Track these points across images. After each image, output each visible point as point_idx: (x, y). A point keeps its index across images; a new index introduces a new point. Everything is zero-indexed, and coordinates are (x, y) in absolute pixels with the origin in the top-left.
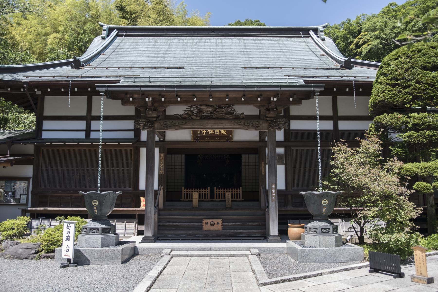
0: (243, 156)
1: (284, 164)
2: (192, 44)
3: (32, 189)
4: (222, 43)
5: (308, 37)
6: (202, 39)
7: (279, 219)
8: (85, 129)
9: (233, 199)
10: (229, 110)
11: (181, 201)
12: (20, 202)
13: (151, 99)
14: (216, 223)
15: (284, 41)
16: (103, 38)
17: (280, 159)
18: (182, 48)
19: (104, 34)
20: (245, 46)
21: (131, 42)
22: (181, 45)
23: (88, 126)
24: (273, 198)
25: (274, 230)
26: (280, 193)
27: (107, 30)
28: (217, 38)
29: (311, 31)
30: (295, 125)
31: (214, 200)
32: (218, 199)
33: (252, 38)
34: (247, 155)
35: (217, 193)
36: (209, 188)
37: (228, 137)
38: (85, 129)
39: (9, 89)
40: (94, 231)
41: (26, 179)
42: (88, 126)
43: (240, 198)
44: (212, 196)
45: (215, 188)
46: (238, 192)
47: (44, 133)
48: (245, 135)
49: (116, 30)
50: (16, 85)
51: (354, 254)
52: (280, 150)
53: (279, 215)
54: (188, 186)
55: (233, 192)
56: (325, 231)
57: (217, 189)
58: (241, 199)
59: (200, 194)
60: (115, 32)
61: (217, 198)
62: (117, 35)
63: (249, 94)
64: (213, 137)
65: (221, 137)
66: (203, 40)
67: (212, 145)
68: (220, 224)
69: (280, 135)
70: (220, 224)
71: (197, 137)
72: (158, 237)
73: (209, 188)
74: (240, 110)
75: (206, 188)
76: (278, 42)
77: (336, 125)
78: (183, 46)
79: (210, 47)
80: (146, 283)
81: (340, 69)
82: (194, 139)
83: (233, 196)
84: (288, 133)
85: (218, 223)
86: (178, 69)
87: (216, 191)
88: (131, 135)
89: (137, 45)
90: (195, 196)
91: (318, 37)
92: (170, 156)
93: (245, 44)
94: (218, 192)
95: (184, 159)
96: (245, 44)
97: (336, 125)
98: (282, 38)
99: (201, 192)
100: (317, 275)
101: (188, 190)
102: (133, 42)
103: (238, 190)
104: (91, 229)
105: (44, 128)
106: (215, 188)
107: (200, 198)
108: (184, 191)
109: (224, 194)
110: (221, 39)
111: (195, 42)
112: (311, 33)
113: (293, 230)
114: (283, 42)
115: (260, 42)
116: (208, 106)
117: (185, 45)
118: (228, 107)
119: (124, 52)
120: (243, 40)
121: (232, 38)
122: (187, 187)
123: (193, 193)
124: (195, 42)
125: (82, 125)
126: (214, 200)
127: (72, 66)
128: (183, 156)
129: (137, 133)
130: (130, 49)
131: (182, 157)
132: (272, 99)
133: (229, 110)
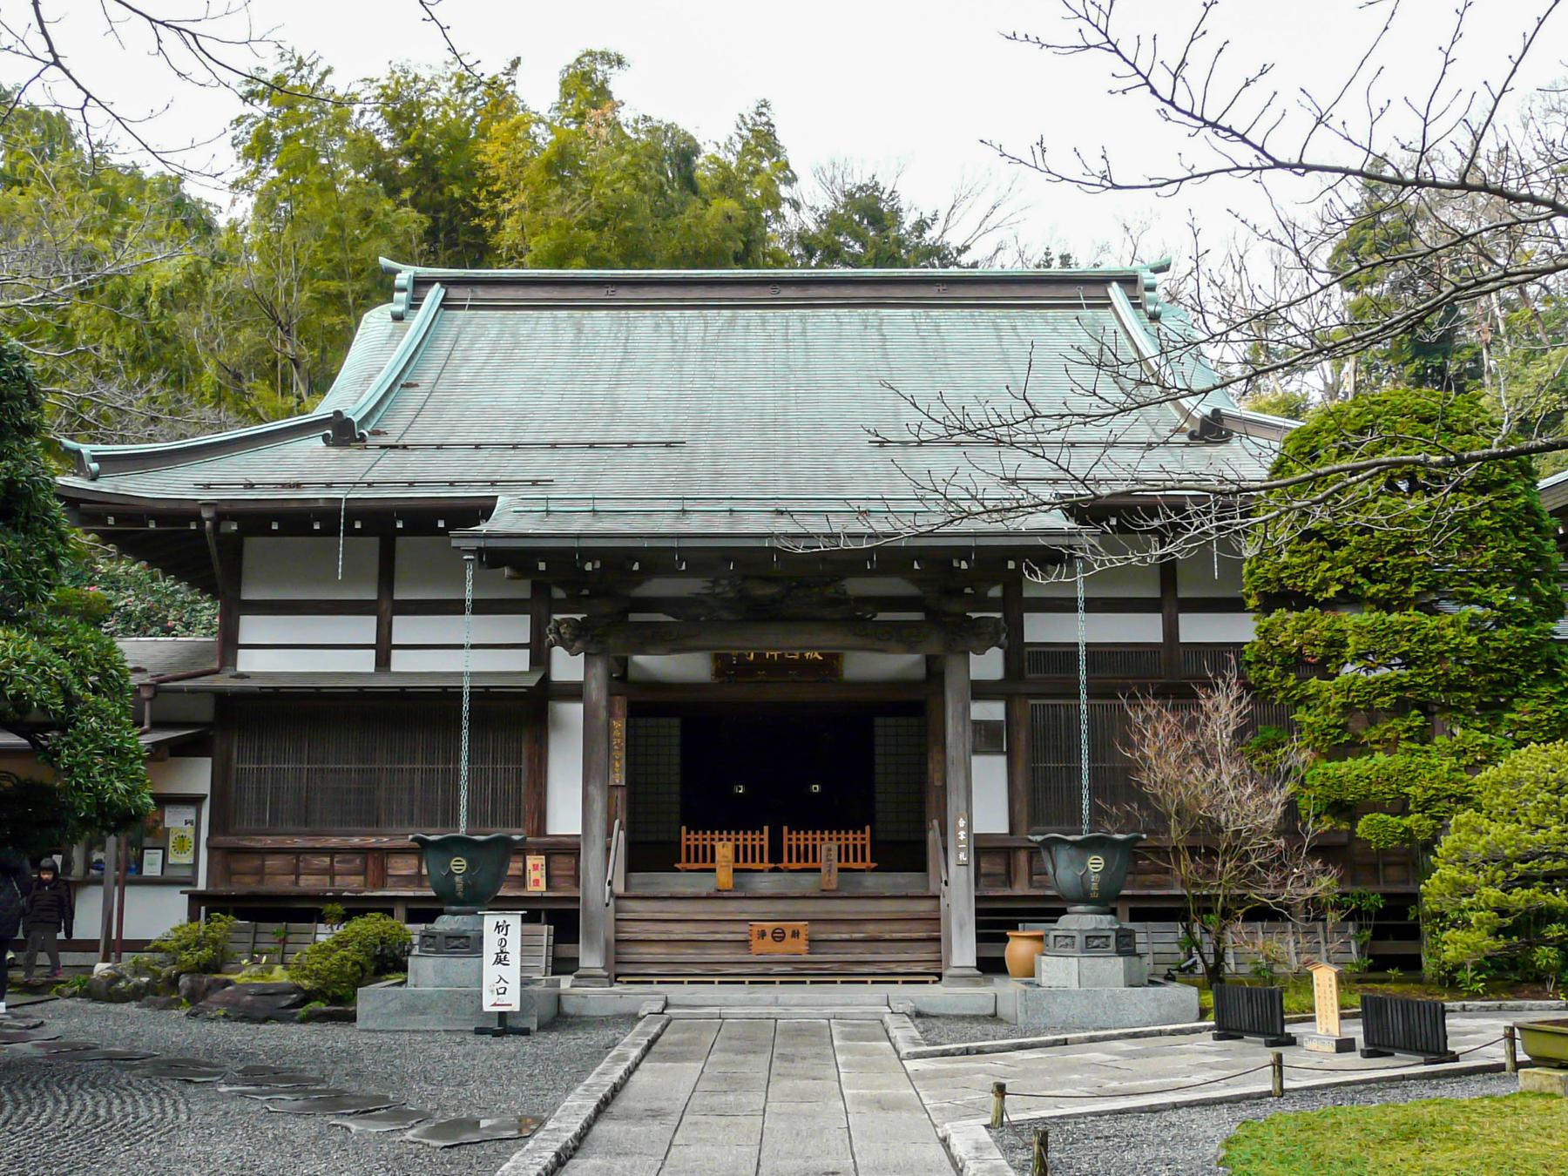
0: (879, 721)
1: (1000, 752)
2: (703, 338)
3: (210, 833)
4: (804, 333)
5: (1105, 306)
6: (734, 318)
7: (979, 925)
8: (394, 652)
9: (844, 865)
10: (830, 591)
11: (678, 870)
12: (141, 871)
13: (598, 565)
14: (788, 933)
15: (1019, 323)
16: (398, 318)
17: (987, 738)
18: (668, 355)
19: (399, 302)
20: (883, 347)
21: (493, 332)
22: (666, 343)
23: (384, 631)
24: (962, 856)
25: (963, 950)
26: (984, 848)
27: (410, 288)
28: (787, 312)
29: (1115, 284)
30: (1040, 629)
31: (781, 866)
32: (794, 865)
33: (908, 311)
34: (891, 721)
35: (688, 847)
36: (766, 828)
37: (831, 663)
38: (394, 652)
39: (152, 526)
40: (456, 943)
41: (195, 801)
42: (384, 631)
43: (863, 860)
44: (776, 855)
45: (785, 829)
46: (859, 843)
47: (242, 654)
48: (897, 664)
49: (437, 285)
50: (177, 516)
51: (1172, 1004)
52: (993, 711)
53: (978, 912)
54: (699, 822)
55: (843, 842)
56: (1096, 942)
57: (790, 832)
58: (869, 864)
59: (737, 847)
60: (434, 294)
61: (790, 860)
62: (446, 305)
63: (890, 558)
64: (783, 666)
65: (804, 665)
66: (741, 322)
67: (775, 693)
68: (802, 936)
69: (988, 665)
70: (802, 936)
71: (723, 665)
72: (617, 976)
73: (766, 828)
74: (856, 586)
75: (756, 827)
76: (997, 328)
77: (1171, 629)
78: (673, 349)
79: (764, 350)
80: (542, 1148)
81: (1187, 445)
82: (718, 672)
83: (843, 853)
84: (1019, 656)
85: (795, 934)
86: (663, 450)
87: (790, 838)
88: (519, 661)
89: (517, 345)
90: (724, 851)
91: (1136, 306)
92: (642, 722)
93: (884, 338)
94: (692, 843)
95: (676, 731)
96: (884, 338)
97: (1171, 629)
98: (1013, 312)
99: (741, 843)
100: (1055, 1043)
101: (700, 836)
102: (502, 332)
103: (757, 835)
104: (448, 937)
105: (241, 641)
106: (785, 829)
107: (737, 860)
108: (688, 838)
109: (814, 847)
110: (802, 318)
111: (713, 330)
112: (1116, 292)
113: (1018, 948)
114: (1014, 328)
115: (937, 329)
116: (769, 580)
117: (680, 346)
118: (827, 584)
119: (477, 374)
120: (876, 322)
121: (840, 311)
122: (694, 827)
123: (719, 846)
124: (713, 330)
125: (364, 628)
126: (781, 866)
127: (325, 438)
128: (676, 722)
129: (540, 658)
130: (495, 361)
131: (672, 727)
132: (955, 564)
133: (830, 591)
